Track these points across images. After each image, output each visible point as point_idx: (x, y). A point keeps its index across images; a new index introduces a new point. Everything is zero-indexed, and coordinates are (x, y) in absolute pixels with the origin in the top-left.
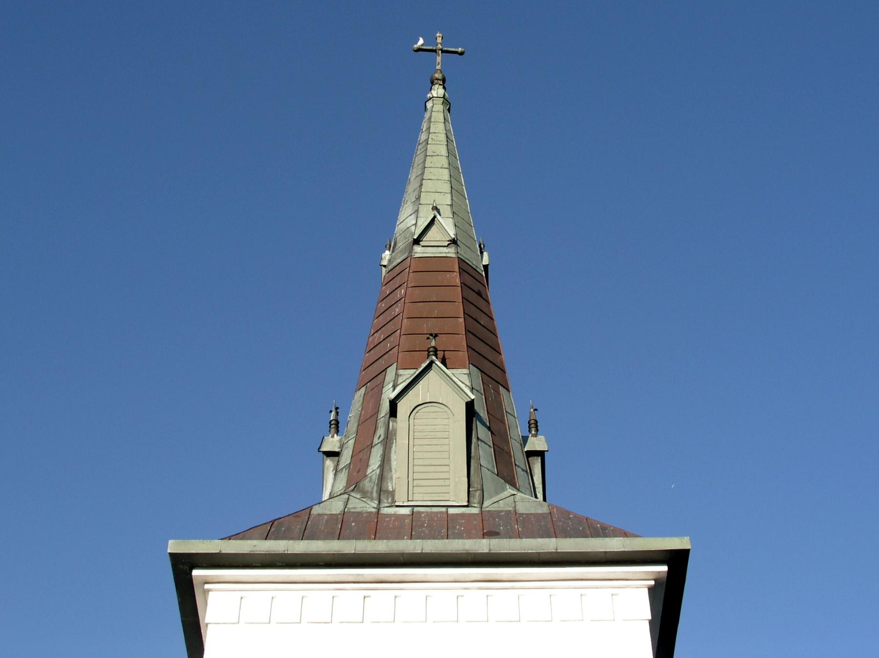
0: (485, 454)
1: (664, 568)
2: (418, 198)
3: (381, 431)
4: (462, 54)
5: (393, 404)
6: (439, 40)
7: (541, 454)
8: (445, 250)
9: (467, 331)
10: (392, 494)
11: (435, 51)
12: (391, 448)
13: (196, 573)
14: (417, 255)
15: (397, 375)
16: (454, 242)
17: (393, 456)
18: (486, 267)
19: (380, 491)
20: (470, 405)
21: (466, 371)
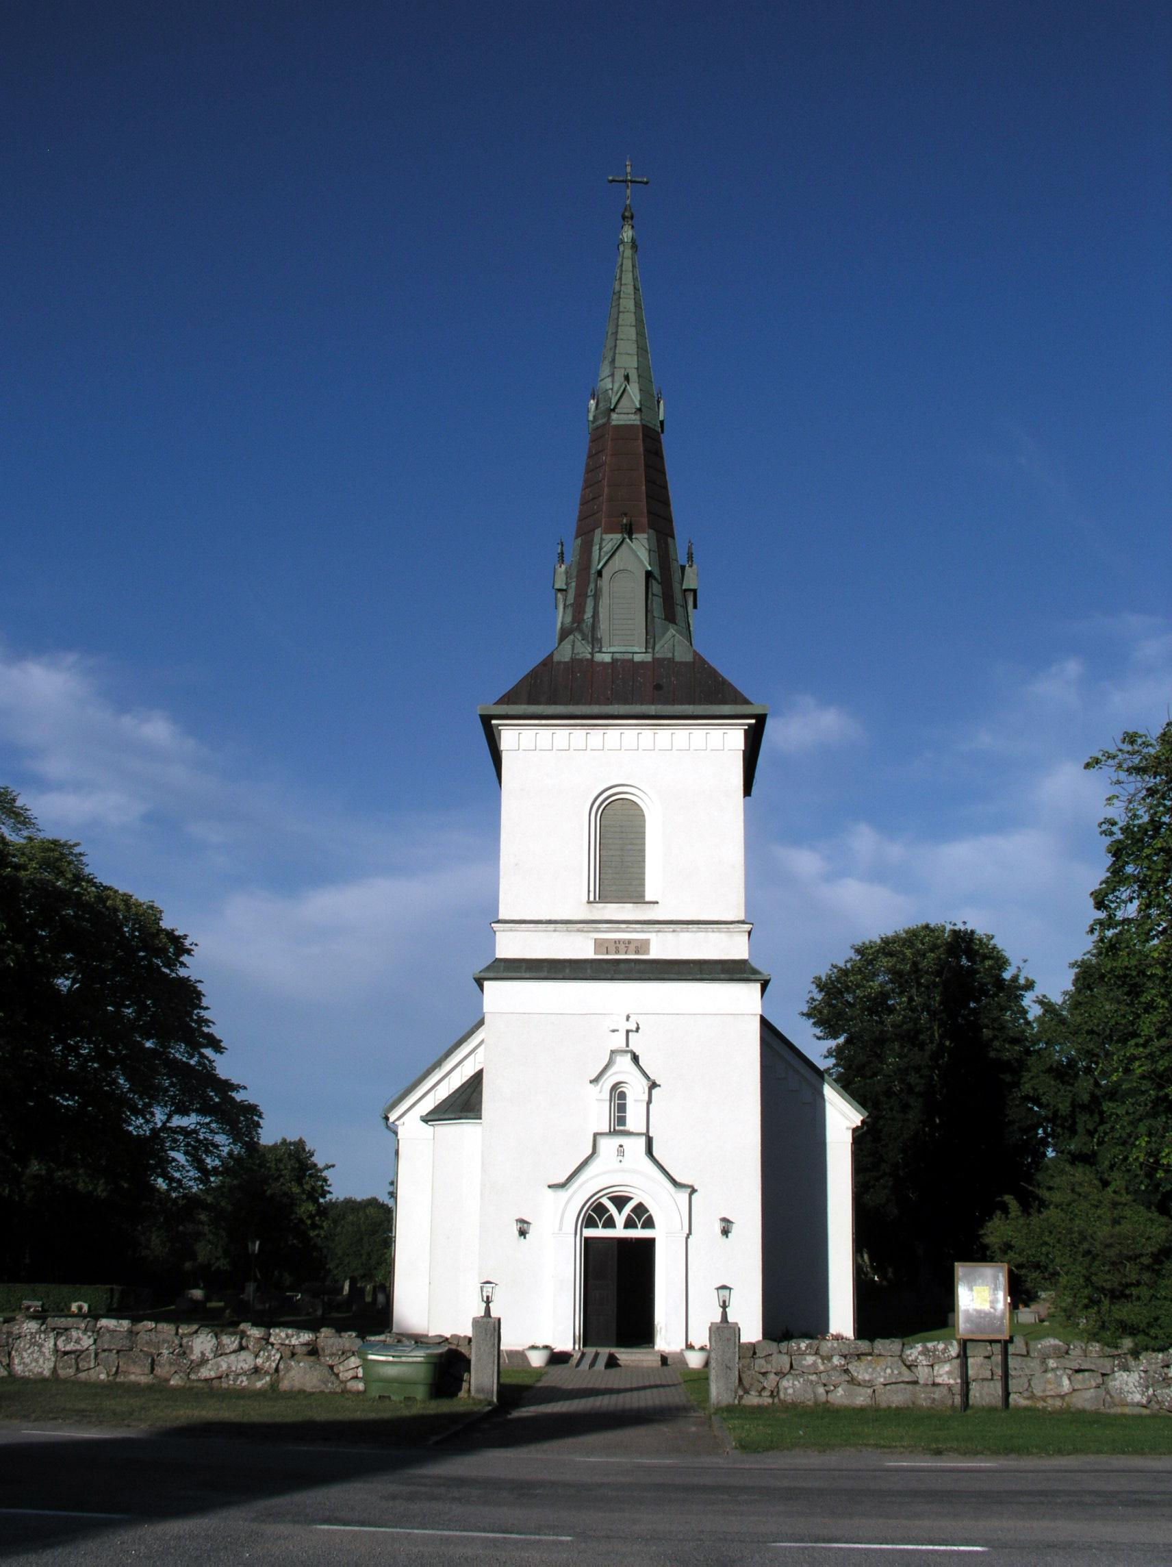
0: (658, 610)
1: (753, 721)
2: (613, 361)
3: (592, 586)
4: (647, 183)
5: (600, 573)
6: (629, 169)
7: (695, 591)
8: (633, 417)
9: (649, 512)
10: (600, 641)
11: (625, 181)
12: (639, 1410)
13: (494, 722)
14: (614, 423)
15: (602, 539)
16: (640, 410)
17: (601, 610)
18: (662, 422)
19: (593, 637)
20: (649, 575)
21: (645, 536)
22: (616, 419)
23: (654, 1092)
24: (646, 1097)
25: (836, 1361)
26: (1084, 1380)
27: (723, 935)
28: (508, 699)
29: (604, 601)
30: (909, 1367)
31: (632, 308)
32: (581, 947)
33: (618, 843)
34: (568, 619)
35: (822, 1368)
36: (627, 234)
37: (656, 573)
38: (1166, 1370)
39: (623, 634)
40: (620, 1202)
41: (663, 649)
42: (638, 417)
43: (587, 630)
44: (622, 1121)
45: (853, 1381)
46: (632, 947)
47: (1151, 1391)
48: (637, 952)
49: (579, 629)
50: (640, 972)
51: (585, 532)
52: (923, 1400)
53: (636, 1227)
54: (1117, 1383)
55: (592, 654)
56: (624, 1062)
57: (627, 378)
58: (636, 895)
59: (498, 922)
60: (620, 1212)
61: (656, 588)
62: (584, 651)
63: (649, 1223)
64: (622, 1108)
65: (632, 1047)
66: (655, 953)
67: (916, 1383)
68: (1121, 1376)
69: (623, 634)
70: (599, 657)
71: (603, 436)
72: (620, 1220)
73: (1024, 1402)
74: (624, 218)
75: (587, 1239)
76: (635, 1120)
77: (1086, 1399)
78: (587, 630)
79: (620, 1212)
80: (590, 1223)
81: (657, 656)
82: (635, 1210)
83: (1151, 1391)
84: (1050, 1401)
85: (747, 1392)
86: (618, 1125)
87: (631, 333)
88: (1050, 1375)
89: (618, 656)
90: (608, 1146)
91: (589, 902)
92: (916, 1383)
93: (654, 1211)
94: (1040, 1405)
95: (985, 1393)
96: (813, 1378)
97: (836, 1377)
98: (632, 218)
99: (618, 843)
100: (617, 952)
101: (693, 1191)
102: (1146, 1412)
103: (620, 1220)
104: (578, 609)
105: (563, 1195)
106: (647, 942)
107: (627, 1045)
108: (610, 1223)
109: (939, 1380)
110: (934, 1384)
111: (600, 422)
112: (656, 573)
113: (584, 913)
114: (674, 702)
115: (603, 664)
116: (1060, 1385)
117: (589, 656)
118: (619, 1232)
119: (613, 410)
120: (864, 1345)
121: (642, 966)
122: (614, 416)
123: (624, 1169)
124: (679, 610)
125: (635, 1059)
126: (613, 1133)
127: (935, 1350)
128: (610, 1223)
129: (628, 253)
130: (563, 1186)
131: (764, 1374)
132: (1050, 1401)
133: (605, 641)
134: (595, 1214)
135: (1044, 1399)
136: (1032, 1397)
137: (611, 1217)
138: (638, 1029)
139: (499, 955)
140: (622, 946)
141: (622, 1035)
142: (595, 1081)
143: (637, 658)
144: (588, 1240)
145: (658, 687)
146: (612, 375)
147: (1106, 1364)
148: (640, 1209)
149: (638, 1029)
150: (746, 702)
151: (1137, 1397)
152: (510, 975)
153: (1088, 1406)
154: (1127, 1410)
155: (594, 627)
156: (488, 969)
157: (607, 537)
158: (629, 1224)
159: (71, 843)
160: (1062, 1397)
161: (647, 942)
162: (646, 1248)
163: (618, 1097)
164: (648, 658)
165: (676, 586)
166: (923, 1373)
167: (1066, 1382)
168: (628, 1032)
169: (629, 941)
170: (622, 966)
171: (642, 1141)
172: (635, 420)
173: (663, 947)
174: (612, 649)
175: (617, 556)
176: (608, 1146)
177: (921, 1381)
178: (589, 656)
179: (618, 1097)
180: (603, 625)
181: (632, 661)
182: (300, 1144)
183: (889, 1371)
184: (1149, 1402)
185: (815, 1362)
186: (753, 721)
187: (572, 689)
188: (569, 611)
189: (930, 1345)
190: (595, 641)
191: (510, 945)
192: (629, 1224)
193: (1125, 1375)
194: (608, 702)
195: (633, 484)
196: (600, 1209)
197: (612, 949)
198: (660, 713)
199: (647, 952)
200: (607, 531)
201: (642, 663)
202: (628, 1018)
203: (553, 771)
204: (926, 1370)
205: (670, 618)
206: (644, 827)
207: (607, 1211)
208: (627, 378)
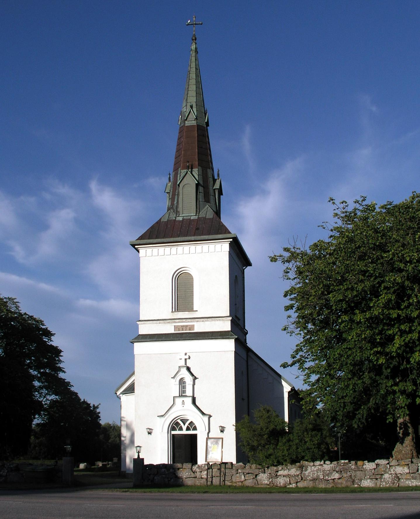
1: (231, 240)
5: (179, 185)
8: (194, 122)
10: (179, 212)
14: (186, 125)
15: (181, 172)
20: (197, 185)
22: (187, 123)
23: (196, 381)
24: (192, 383)
26: (249, 476)
27: (221, 322)
28: (141, 238)
29: (181, 197)
30: (194, 472)
31: (194, 77)
32: (169, 329)
33: (183, 290)
34: (170, 204)
35: (167, 473)
36: (193, 47)
37: (201, 183)
39: (188, 210)
40: (184, 421)
41: (202, 214)
42: (195, 122)
43: (175, 208)
44: (184, 392)
46: (188, 328)
47: (271, 480)
48: (190, 330)
49: (172, 208)
50: (190, 337)
51: (176, 170)
52: (198, 483)
54: (260, 477)
55: (176, 218)
56: (184, 370)
57: (192, 107)
58: (190, 309)
59: (140, 321)
60: (184, 425)
61: (201, 189)
62: (173, 217)
63: (195, 429)
64: (184, 387)
65: (188, 365)
66: (196, 330)
67: (196, 477)
68: (261, 475)
69: (188, 210)
70: (178, 219)
71: (184, 130)
72: (184, 428)
73: (229, 484)
74: (192, 39)
75: (173, 435)
76: (189, 391)
77: (250, 482)
78: (175, 208)
79: (184, 425)
80: (173, 429)
81: (200, 216)
82: (189, 424)
83: (271, 480)
84: (238, 483)
86: (182, 394)
87: (194, 87)
88: (238, 475)
90: (179, 401)
91: (172, 312)
92: (196, 477)
93: (197, 424)
94: (234, 485)
95: (216, 481)
96: (164, 476)
98: (196, 39)
99: (183, 290)
100: (183, 330)
101: (210, 416)
102: (268, 486)
103: (184, 428)
104: (172, 199)
105: (163, 419)
106: (193, 326)
107: (186, 364)
108: (181, 429)
109: (203, 477)
110: (201, 478)
111: (182, 125)
112: (201, 183)
113: (170, 316)
114: (202, 235)
115: (179, 221)
116: (241, 478)
118: (184, 432)
119: (186, 120)
121: (178, 335)
122: (186, 122)
123: (185, 410)
124: (212, 198)
125: (188, 369)
126: (181, 396)
128: (181, 429)
129: (194, 54)
130: (162, 416)
131: (150, 475)
132: (238, 483)
133: (181, 213)
134: (175, 425)
135: (236, 483)
136: (232, 482)
138: (189, 358)
139: (140, 333)
141: (183, 361)
142: (173, 378)
143: (192, 218)
144: (174, 435)
145: (197, 229)
146: (186, 105)
147: (257, 472)
149: (189, 358)
150: (230, 233)
151: (266, 482)
152: (143, 340)
153: (250, 485)
154: (262, 486)
155: (177, 207)
156: (135, 338)
158: (188, 429)
159: (13, 298)
160: (242, 482)
161: (193, 326)
162: (194, 438)
163: (182, 382)
164: (196, 217)
165: (211, 187)
166: (198, 474)
167: (243, 477)
168: (186, 359)
169: (187, 326)
170: (184, 335)
171: (191, 399)
172: (194, 123)
173: (199, 327)
174: (183, 215)
175: (185, 179)
179: (182, 382)
180: (180, 206)
181: (190, 219)
184: (270, 483)
186: (231, 240)
187: (162, 232)
188: (170, 200)
190: (177, 213)
191: (144, 329)
192: (188, 429)
193: (262, 474)
194: (179, 236)
195: (197, 150)
196: (177, 424)
197: (181, 329)
198: (141, 243)
200: (183, 169)
202: (186, 354)
203: (159, 263)
204: (199, 473)
205: (207, 200)
206: (193, 282)
208: (192, 107)
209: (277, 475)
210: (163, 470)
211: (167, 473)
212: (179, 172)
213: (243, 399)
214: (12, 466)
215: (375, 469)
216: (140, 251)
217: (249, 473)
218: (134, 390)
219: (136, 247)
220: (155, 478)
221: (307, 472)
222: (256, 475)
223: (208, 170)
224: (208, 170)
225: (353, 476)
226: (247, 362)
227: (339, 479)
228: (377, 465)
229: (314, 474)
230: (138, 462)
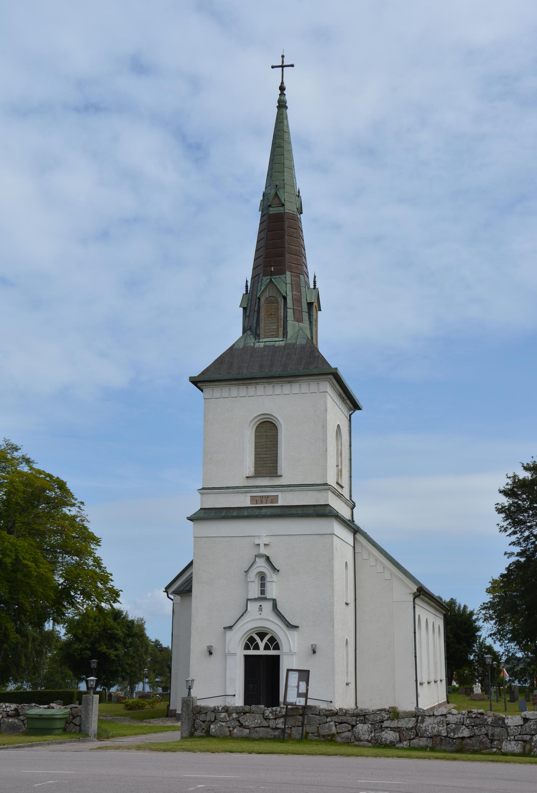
15: (262, 279)
25: (235, 715)
35: (228, 719)
38: (382, 724)
40: (262, 635)
43: (254, 330)
45: (241, 725)
46: (269, 499)
48: (272, 503)
53: (270, 649)
58: (273, 472)
60: (262, 641)
63: (277, 647)
68: (360, 726)
72: (262, 645)
78: (254, 330)
79: (262, 641)
83: (373, 734)
85: (196, 730)
89: (267, 344)
90: (253, 607)
97: (234, 723)
100: (262, 503)
103: (262, 645)
108: (257, 647)
117: (252, 345)
118: (262, 652)
120: (247, 708)
127: (276, 711)
128: (257, 647)
134: (251, 643)
137: (257, 644)
140: (264, 500)
148: (272, 640)
157: (264, 278)
158: (267, 647)
167: (334, 728)
169: (268, 497)
173: (285, 499)
174: (265, 340)
176: (253, 607)
177: (271, 727)
178: (252, 345)
182: (452, 599)
183: (256, 721)
185: (225, 717)
189: (274, 708)
192: (267, 647)
199: (278, 503)
200: (264, 276)
201: (279, 347)
207: (256, 641)
209: (381, 727)
210: (223, 715)
211: (228, 719)
212: (260, 280)
213: (347, 604)
214: (8, 709)
215: (522, 725)
216: (204, 389)
217: (341, 723)
218: (190, 591)
219: (199, 385)
220: (212, 726)
221: (424, 724)
222: (353, 726)
223: (301, 276)
224: (301, 276)
225: (489, 734)
226: (354, 547)
227: (470, 737)
228: (526, 720)
229: (434, 728)
230: (187, 702)
